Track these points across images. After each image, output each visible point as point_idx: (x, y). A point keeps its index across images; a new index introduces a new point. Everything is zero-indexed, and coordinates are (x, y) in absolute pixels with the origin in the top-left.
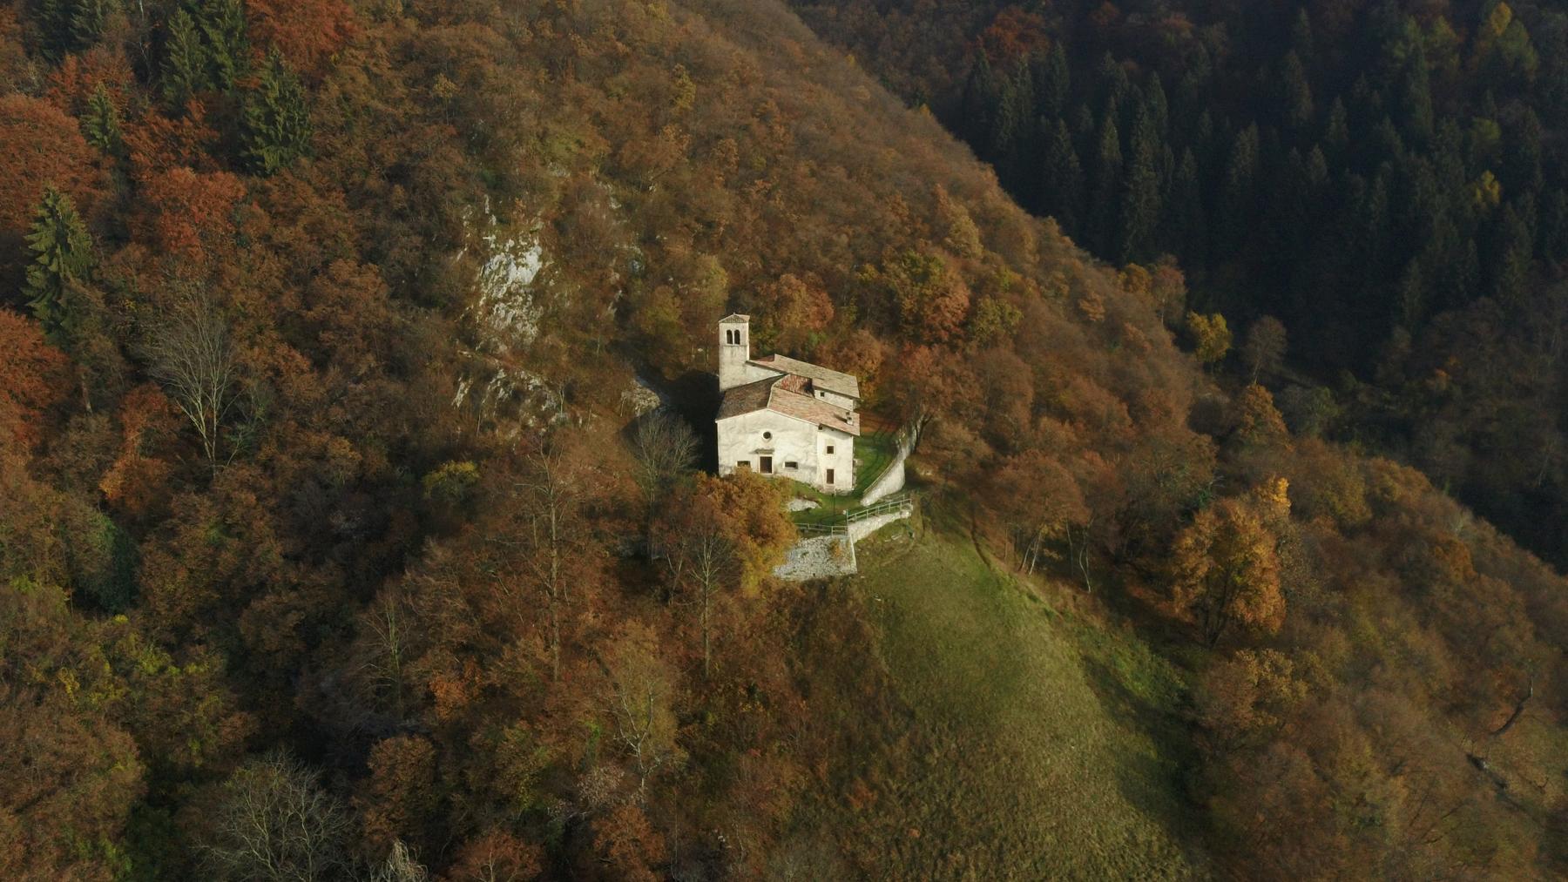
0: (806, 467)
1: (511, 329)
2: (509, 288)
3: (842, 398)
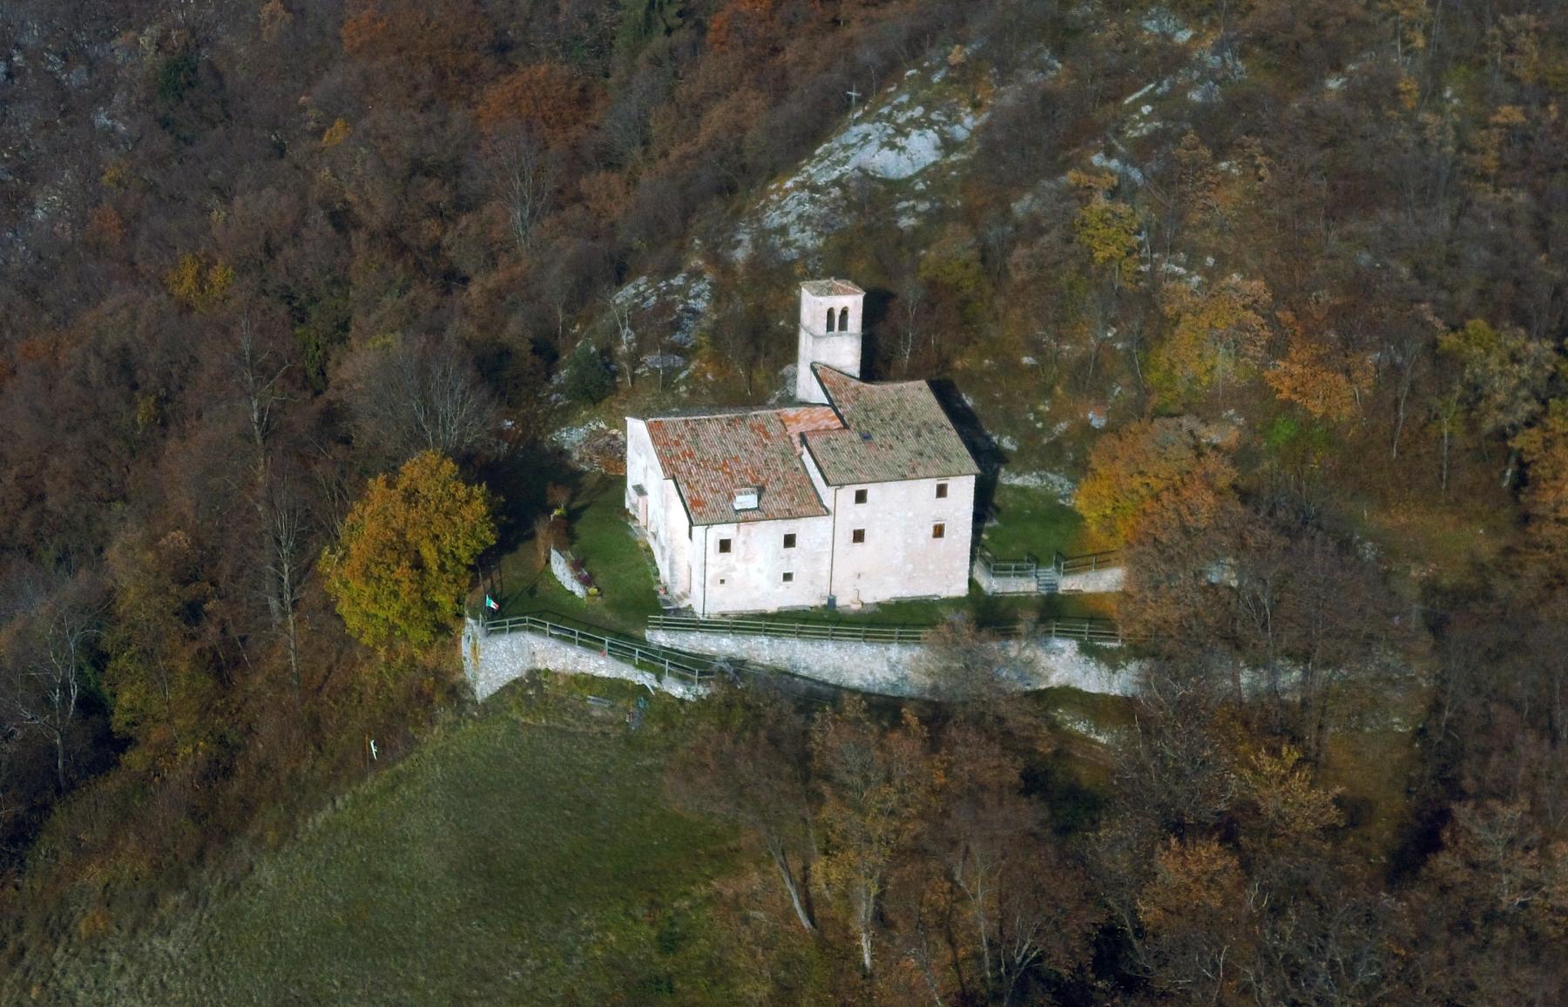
0: (660, 544)
1: (783, 230)
2: (843, 175)
3: (819, 476)
